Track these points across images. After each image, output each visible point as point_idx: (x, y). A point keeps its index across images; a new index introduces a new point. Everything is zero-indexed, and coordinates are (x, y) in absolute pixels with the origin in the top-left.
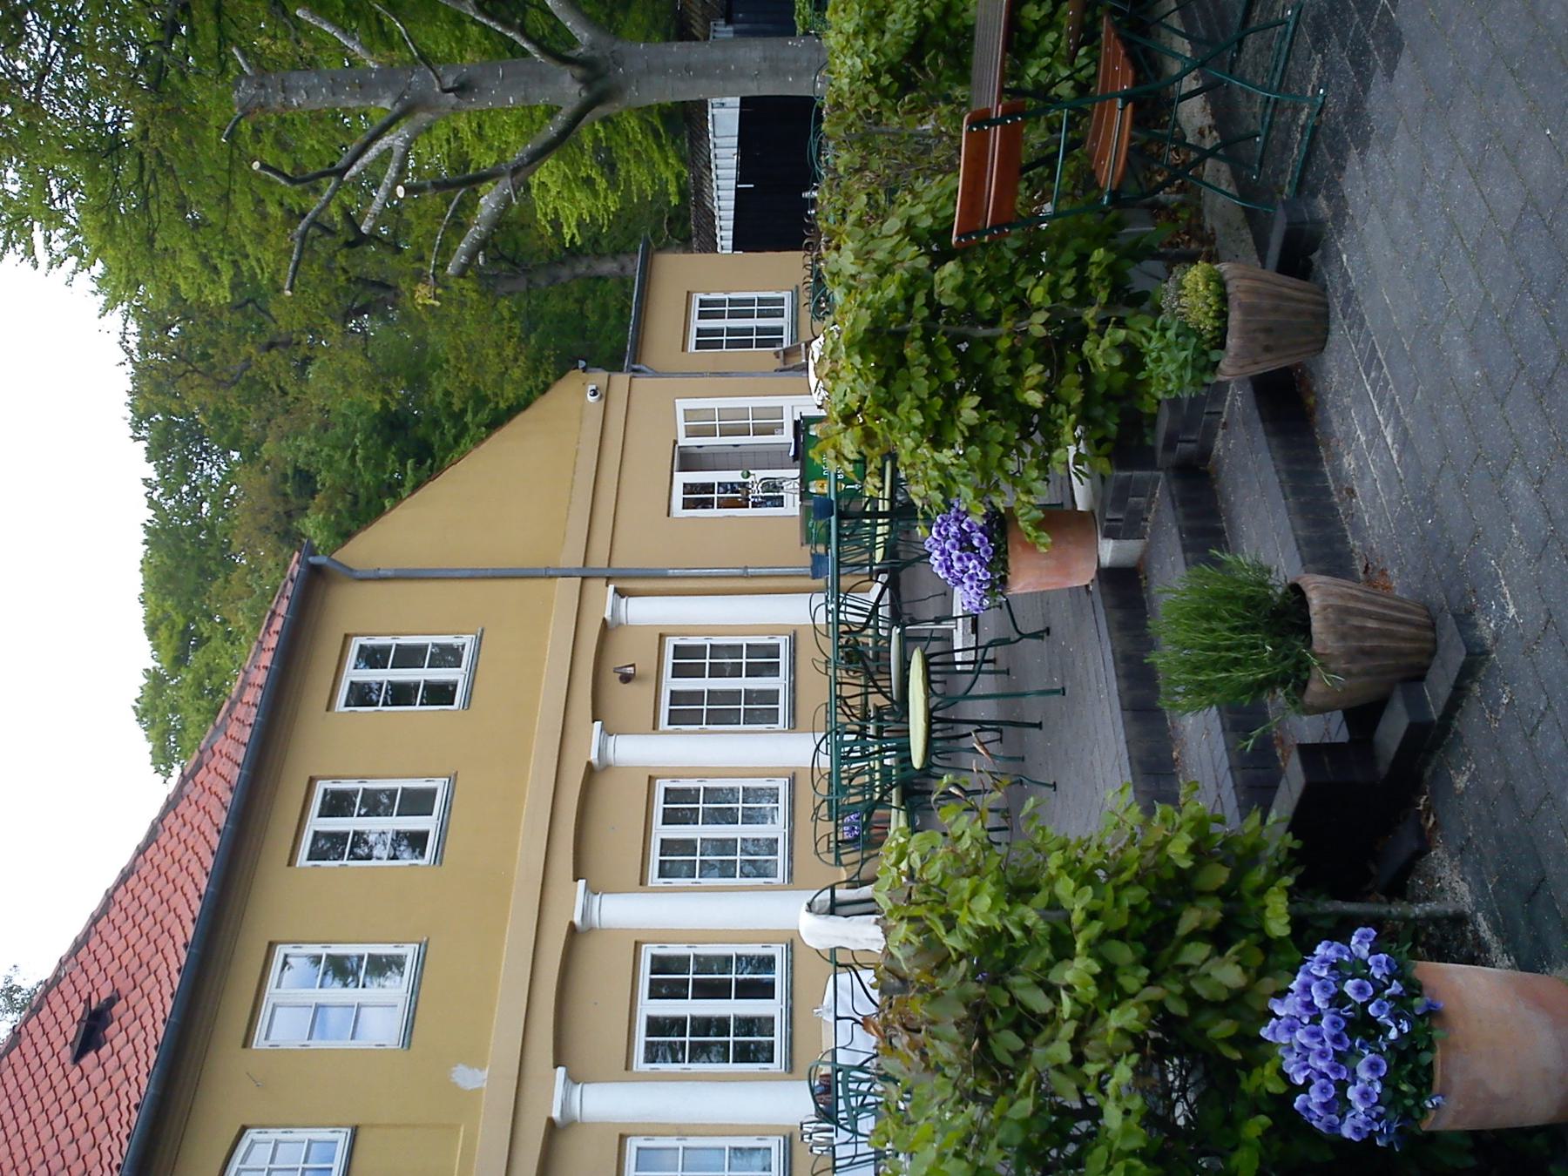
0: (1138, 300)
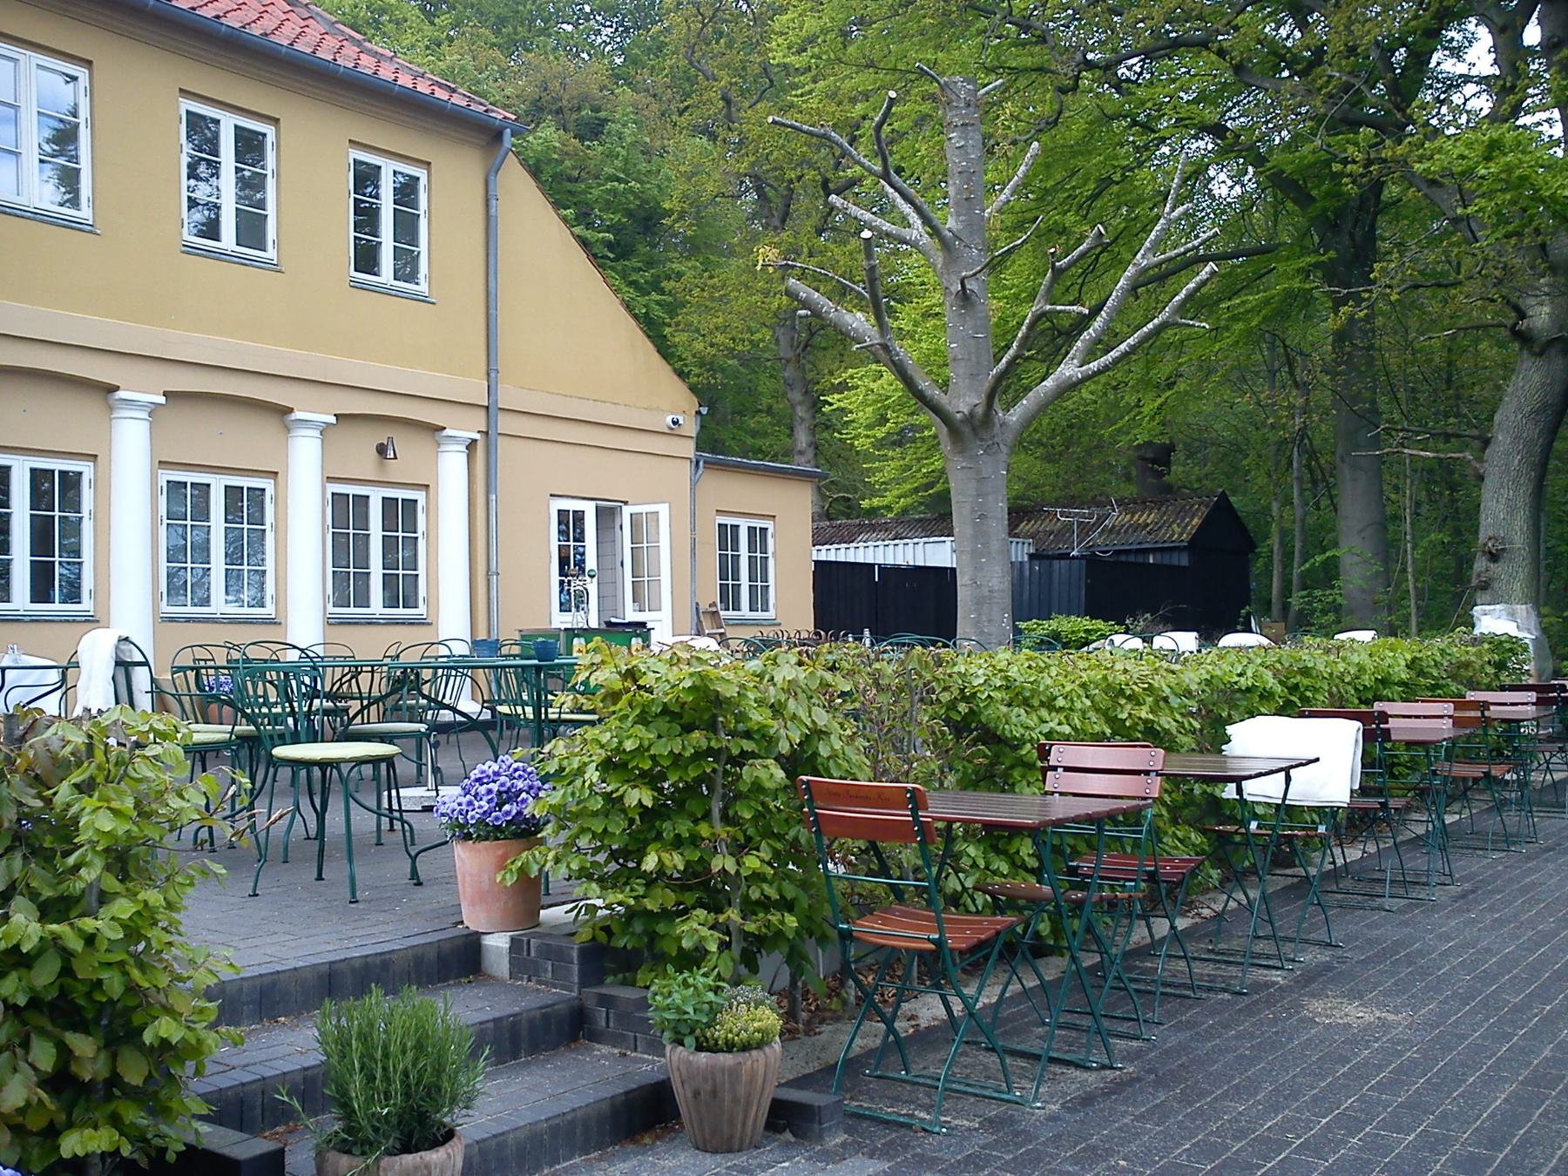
0: (749, 961)
